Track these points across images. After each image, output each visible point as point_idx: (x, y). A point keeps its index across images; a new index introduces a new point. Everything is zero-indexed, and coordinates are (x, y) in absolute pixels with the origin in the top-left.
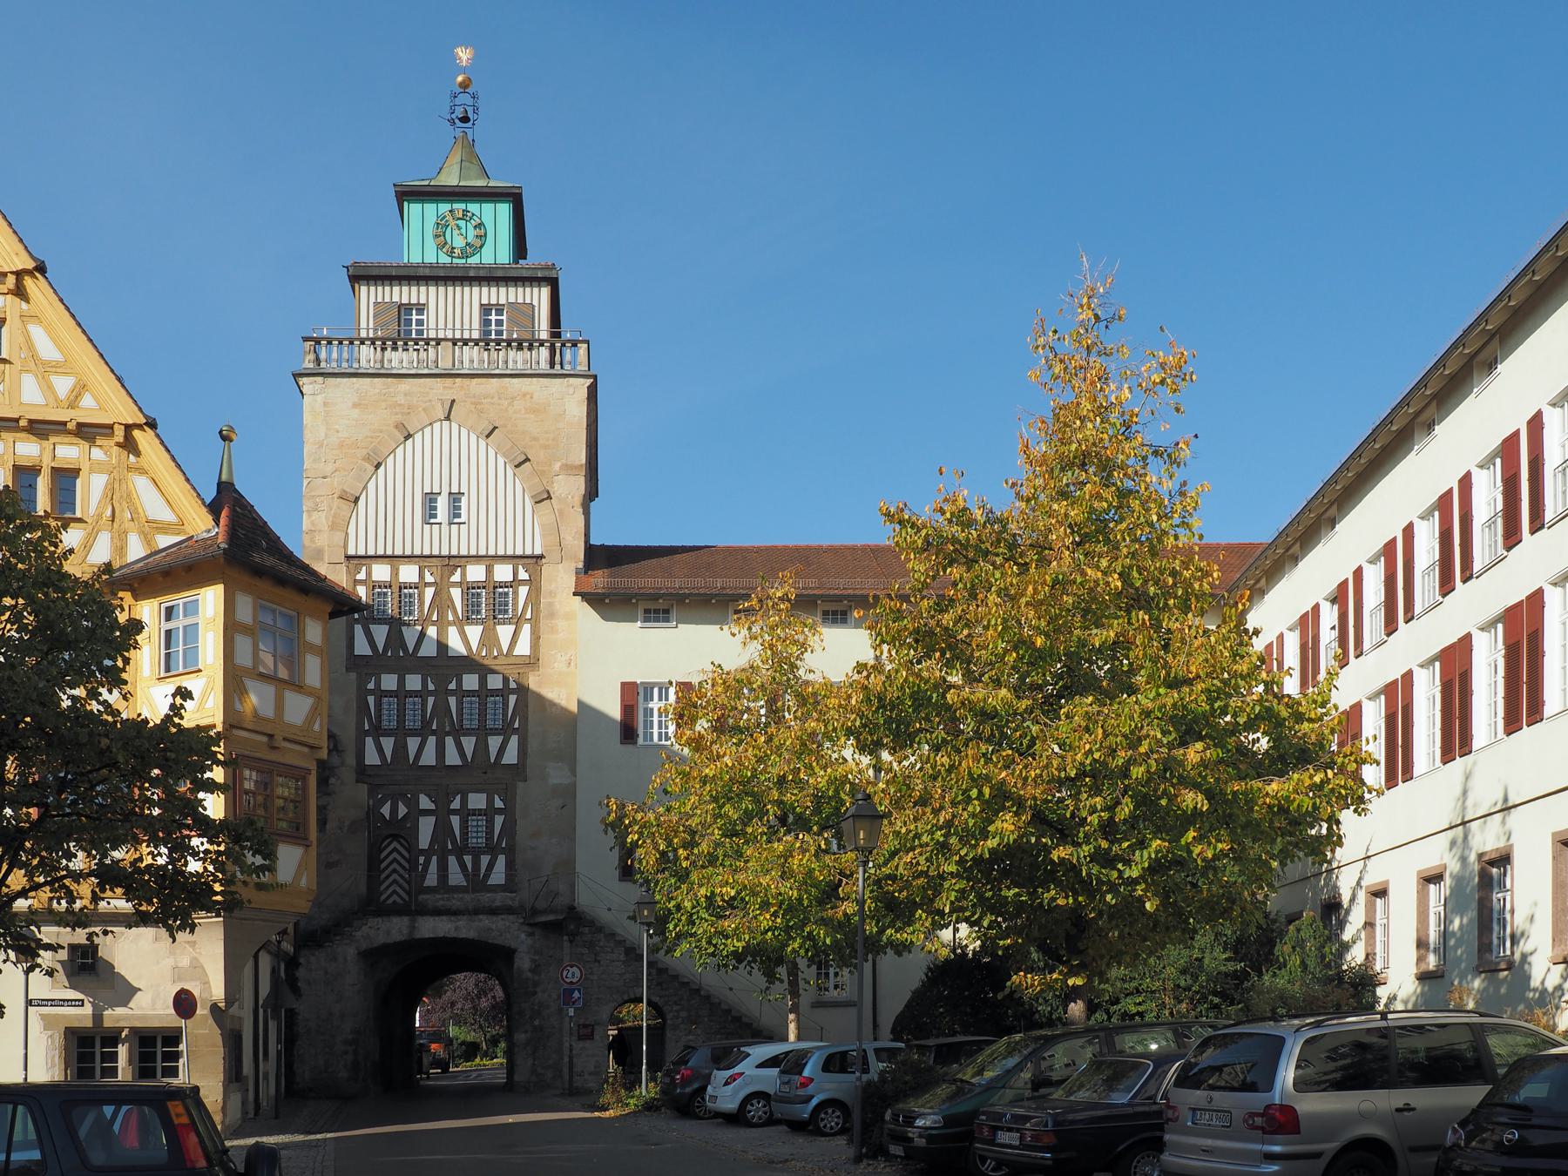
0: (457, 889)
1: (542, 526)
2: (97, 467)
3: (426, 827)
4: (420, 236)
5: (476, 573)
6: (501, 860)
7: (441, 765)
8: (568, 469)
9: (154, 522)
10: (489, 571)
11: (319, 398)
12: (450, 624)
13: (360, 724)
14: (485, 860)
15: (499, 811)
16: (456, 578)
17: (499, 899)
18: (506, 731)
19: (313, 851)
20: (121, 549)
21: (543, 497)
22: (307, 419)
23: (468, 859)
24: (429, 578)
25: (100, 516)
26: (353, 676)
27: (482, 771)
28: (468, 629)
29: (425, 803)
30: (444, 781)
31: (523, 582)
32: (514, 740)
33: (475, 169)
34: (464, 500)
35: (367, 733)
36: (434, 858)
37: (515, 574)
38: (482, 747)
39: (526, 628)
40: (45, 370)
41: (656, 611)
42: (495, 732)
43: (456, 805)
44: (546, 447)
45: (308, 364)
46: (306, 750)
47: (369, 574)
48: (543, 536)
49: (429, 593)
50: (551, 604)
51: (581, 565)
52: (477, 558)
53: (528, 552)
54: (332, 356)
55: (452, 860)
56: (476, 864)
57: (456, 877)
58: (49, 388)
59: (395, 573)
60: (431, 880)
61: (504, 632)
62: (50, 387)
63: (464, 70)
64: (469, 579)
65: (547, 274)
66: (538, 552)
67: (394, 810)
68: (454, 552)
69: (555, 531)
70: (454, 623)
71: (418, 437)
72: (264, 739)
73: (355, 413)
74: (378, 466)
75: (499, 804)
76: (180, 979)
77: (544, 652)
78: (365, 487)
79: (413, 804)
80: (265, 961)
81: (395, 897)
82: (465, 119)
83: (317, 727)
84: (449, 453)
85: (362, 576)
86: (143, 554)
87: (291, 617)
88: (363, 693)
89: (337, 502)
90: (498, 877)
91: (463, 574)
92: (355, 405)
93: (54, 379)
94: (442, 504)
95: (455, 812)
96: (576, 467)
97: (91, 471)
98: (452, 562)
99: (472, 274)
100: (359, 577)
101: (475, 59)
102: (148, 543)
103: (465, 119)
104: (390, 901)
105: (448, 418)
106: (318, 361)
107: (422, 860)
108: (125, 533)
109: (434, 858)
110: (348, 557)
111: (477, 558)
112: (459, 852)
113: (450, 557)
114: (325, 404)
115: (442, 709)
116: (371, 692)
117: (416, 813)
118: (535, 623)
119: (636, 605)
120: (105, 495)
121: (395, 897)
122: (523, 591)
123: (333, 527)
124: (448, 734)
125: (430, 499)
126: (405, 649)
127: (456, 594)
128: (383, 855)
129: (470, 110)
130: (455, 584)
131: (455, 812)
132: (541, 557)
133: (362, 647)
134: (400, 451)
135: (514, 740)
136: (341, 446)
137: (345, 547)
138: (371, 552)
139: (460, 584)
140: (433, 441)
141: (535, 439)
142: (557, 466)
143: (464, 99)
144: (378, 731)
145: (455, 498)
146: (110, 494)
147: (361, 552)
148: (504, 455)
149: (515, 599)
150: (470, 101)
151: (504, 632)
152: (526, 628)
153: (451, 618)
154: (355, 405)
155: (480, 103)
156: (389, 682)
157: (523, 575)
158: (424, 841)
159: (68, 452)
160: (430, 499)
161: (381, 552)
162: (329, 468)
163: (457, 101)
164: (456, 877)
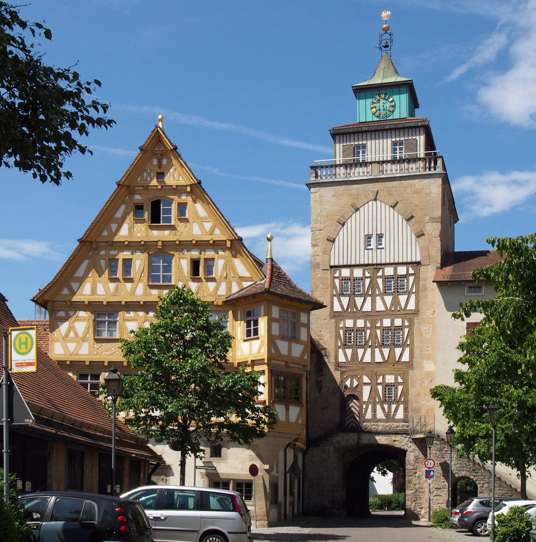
0: (380, 420)
1: (420, 247)
2: (222, 257)
3: (366, 391)
4: (365, 111)
5: (389, 271)
6: (401, 407)
7: (373, 363)
8: (433, 220)
9: (242, 277)
10: (395, 270)
11: (317, 194)
12: (377, 295)
13: (336, 343)
14: (394, 407)
15: (400, 384)
16: (380, 273)
17: (401, 426)
18: (403, 346)
19: (304, 408)
20: (229, 288)
21: (420, 235)
22: (312, 204)
23: (386, 406)
24: (367, 275)
25: (222, 276)
26: (333, 320)
27: (391, 363)
28: (385, 297)
29: (366, 380)
30: (374, 369)
31: (411, 275)
32: (407, 350)
33: (391, 70)
34: (383, 239)
35: (339, 347)
36: (370, 406)
37: (408, 271)
38: (392, 353)
39: (413, 297)
40: (201, 221)
41: (475, 287)
42: (398, 346)
43: (380, 380)
44: (422, 209)
45: (313, 179)
46: (301, 366)
47: (340, 274)
48: (421, 252)
49: (367, 281)
50: (425, 285)
51: (439, 265)
52: (390, 264)
53: (414, 260)
54: (324, 176)
55: (378, 407)
56: (389, 408)
57: (380, 415)
58: (202, 228)
59: (352, 273)
60: (369, 416)
61: (403, 299)
62: (204, 227)
63: (386, 22)
64: (386, 274)
65: (423, 123)
66: (418, 260)
67: (352, 383)
68: (379, 262)
69: (425, 250)
70: (379, 295)
71: (362, 209)
72: (284, 363)
73: (334, 200)
74: (343, 225)
75: (400, 380)
76: (252, 460)
77: (421, 307)
78: (338, 234)
79: (360, 380)
80: (290, 453)
81: (352, 424)
82: (386, 46)
83: (305, 357)
84: (376, 215)
85: (337, 275)
86: (238, 290)
87: (295, 313)
88: (337, 328)
89: (326, 241)
90: (400, 415)
91: (383, 272)
92: (334, 196)
93: (205, 224)
94: (373, 241)
95: (380, 384)
96: (436, 218)
97: (218, 258)
98: (379, 266)
99: (387, 127)
100: (336, 275)
101: (391, 16)
102: (240, 286)
103: (386, 46)
104: (350, 425)
105: (375, 200)
106: (316, 176)
107: (364, 406)
108: (231, 282)
109: (370, 406)
110: (331, 267)
111: (390, 264)
112: (382, 403)
113: (377, 264)
114: (320, 197)
115: (373, 336)
116: (342, 328)
117: (362, 384)
118: (417, 293)
119: (464, 285)
120: (223, 268)
121: (352, 424)
122: (411, 279)
123: (324, 253)
124: (377, 347)
125: (368, 237)
126: (357, 308)
127: (380, 281)
128: (347, 419)
129: (389, 41)
130: (379, 277)
131: (380, 384)
132: (419, 263)
133: (337, 308)
134: (353, 216)
135: (407, 350)
136: (327, 215)
137: (330, 261)
138: (341, 264)
139: (381, 277)
140: (370, 210)
141: (416, 206)
142: (427, 218)
143: (387, 36)
144: (345, 346)
145: (380, 237)
146: (225, 268)
147: (337, 264)
148: (401, 215)
149: (408, 283)
150: (389, 37)
151: (403, 299)
152: (413, 297)
153: (377, 293)
154: (334, 196)
155: (394, 37)
156: (349, 323)
157: (411, 271)
158: (365, 398)
159: (210, 254)
160: (368, 237)
161: (345, 263)
162: (322, 226)
163: (383, 38)
164: (380, 415)
